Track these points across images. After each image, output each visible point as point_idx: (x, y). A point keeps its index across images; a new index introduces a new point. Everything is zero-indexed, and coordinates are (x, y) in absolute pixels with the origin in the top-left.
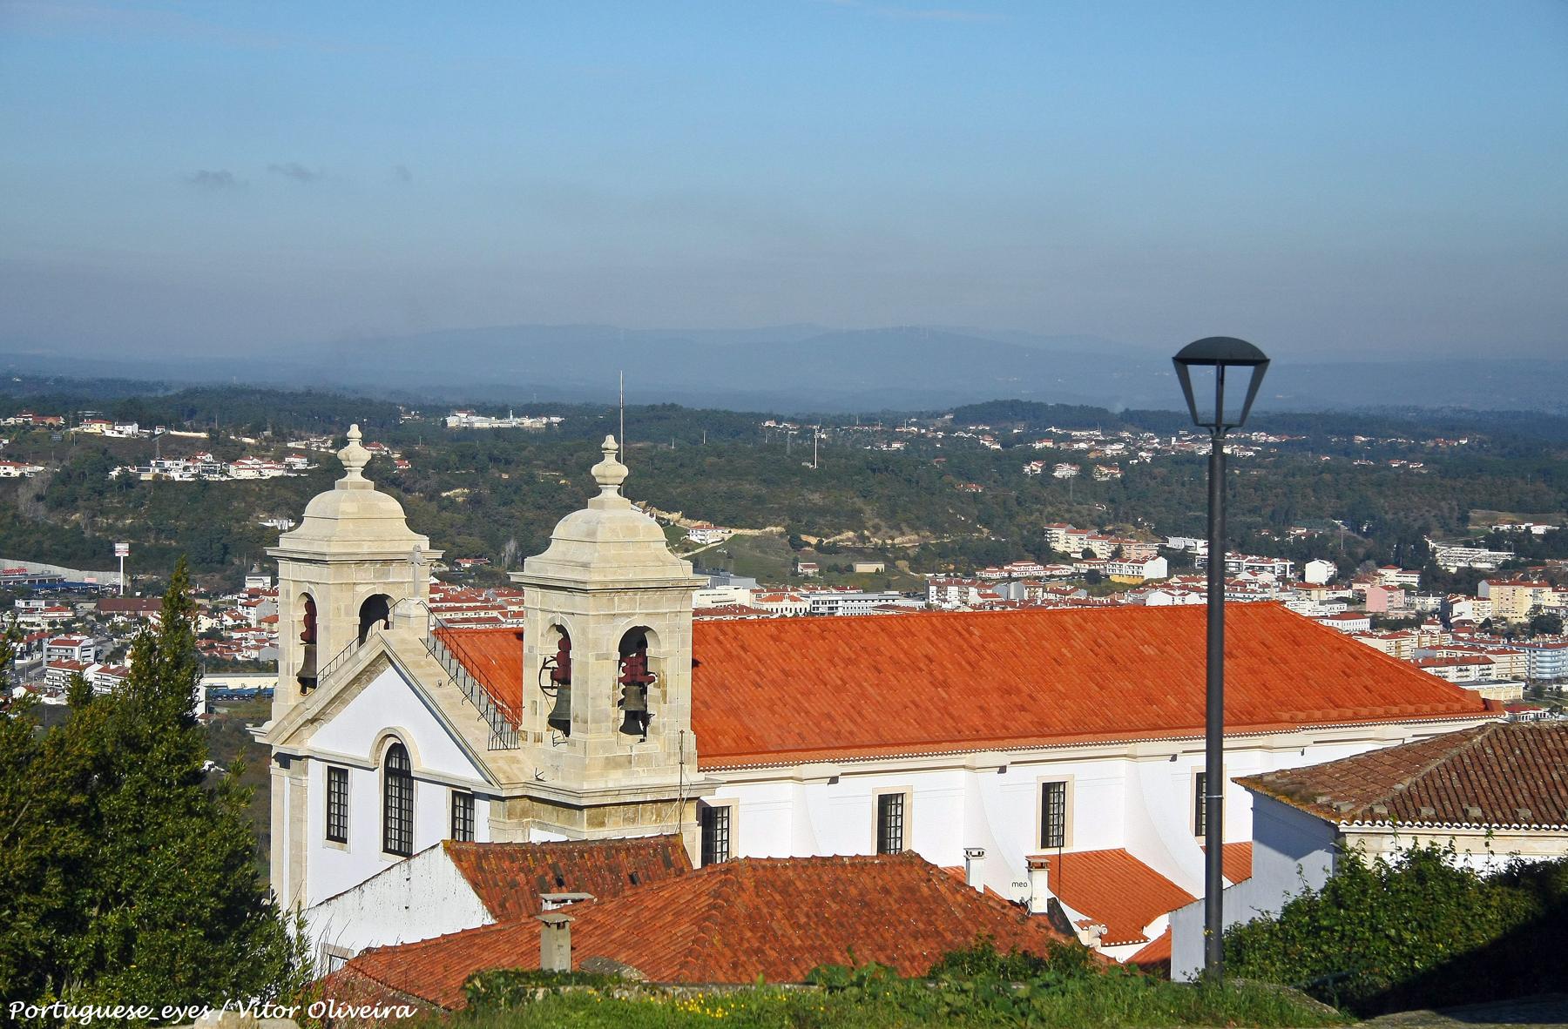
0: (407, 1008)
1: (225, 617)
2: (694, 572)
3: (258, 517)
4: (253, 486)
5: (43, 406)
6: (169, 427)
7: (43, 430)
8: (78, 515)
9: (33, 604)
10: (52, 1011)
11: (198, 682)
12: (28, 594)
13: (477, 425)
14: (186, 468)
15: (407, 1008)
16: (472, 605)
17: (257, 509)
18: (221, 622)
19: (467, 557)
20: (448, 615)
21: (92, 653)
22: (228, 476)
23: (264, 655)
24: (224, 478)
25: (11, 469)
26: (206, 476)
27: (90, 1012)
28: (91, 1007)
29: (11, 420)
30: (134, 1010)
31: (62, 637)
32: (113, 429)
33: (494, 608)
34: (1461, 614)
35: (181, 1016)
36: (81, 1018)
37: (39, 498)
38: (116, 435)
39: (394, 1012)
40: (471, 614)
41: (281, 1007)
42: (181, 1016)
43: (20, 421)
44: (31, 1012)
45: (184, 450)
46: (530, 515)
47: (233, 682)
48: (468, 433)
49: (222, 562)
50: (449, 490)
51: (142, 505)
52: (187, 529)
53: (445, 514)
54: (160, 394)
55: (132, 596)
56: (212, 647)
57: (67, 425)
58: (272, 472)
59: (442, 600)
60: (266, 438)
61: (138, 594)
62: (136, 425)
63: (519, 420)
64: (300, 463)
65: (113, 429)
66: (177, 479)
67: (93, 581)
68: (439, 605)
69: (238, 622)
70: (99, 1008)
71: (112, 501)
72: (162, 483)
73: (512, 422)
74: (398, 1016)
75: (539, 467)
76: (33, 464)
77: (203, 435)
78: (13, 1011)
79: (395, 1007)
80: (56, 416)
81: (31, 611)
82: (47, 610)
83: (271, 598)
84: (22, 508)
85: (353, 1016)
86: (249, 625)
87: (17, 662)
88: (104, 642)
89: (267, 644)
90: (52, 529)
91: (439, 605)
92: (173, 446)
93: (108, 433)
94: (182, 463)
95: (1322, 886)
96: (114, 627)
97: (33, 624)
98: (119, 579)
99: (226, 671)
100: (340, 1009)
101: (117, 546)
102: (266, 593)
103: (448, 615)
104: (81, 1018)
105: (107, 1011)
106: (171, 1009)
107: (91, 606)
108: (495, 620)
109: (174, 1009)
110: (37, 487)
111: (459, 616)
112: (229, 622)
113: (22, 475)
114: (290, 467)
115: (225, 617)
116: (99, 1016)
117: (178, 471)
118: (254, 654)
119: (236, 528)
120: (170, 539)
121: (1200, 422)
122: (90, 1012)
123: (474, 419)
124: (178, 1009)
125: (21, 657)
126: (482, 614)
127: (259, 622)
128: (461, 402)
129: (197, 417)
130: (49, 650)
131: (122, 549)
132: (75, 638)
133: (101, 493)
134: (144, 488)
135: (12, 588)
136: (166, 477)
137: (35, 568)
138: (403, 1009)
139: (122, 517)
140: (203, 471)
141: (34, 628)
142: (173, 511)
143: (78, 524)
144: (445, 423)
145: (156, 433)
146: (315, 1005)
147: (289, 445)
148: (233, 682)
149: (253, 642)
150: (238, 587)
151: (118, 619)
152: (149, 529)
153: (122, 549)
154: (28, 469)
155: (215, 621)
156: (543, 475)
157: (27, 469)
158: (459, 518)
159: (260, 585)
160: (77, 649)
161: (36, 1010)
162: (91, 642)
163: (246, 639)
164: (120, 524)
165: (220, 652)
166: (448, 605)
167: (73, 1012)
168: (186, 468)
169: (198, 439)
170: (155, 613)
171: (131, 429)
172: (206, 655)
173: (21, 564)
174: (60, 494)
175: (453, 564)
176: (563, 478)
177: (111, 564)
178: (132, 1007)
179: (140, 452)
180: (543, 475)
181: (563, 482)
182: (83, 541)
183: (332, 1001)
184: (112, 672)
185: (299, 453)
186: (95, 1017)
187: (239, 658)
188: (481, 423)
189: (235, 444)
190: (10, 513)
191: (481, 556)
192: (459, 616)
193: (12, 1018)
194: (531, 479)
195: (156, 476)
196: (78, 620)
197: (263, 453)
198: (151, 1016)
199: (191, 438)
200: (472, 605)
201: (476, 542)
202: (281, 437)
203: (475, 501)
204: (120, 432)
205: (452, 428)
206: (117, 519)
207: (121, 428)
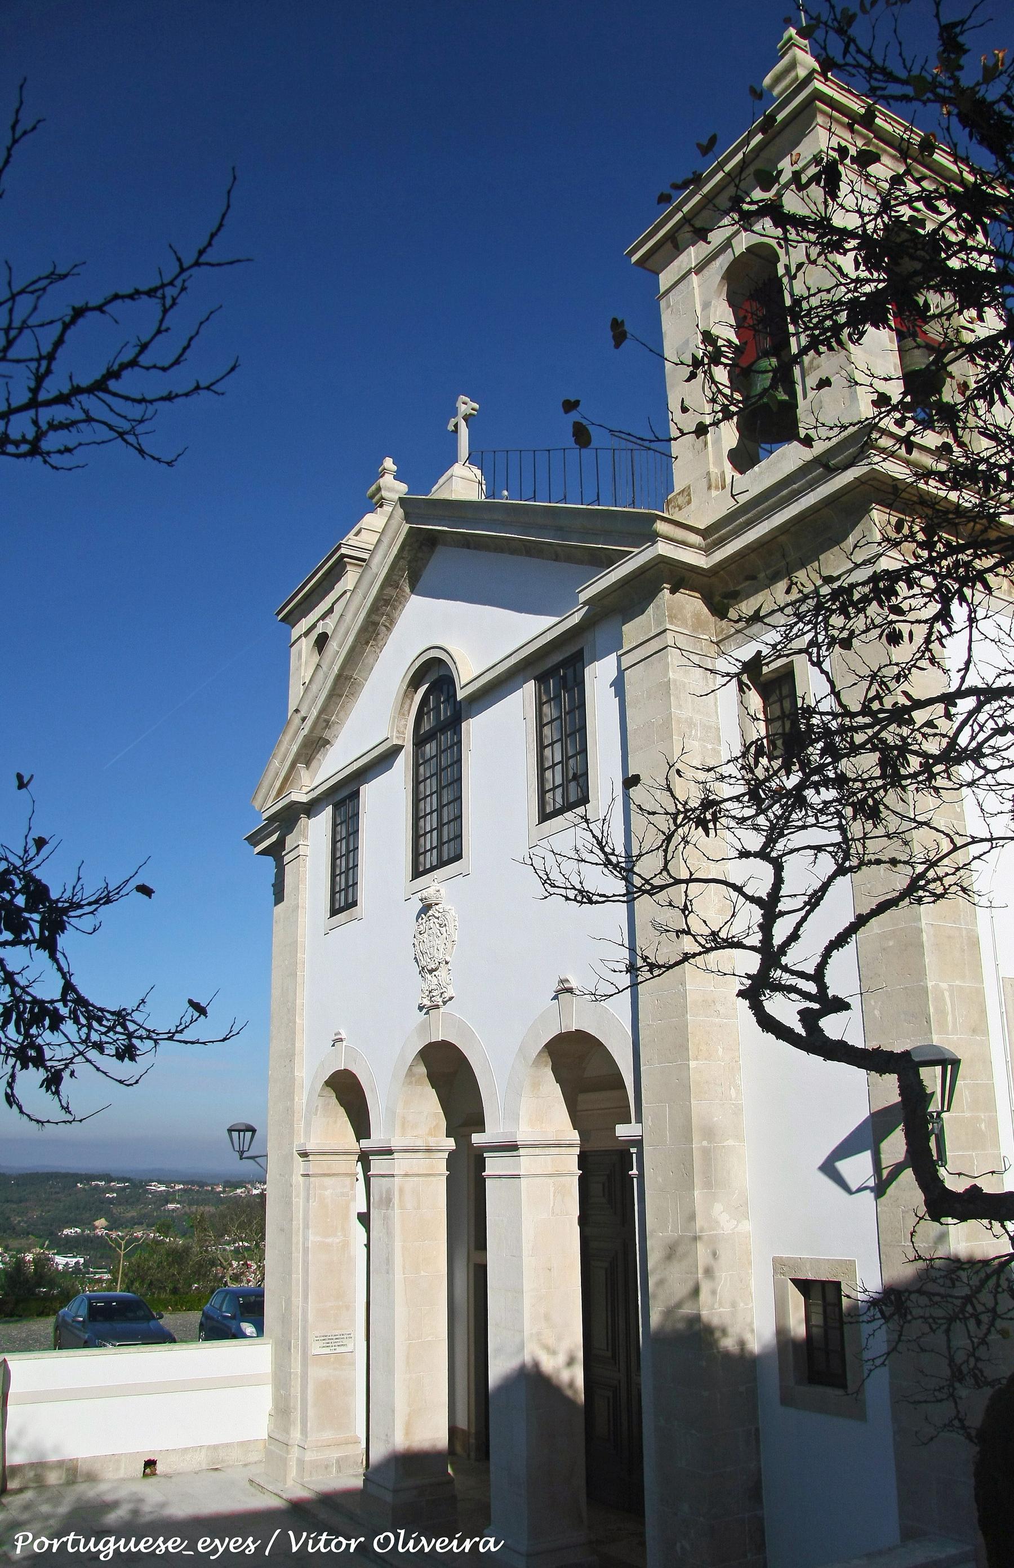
0: (492, 1540)
2: (839, 1283)
10: (66, 1543)
11: (985, 1378)
28: (112, 1539)
30: (164, 1542)
35: (221, 1550)
39: (477, 1544)
44: (339, 1545)
70: (123, 1540)
74: (482, 1550)
78: (20, 1544)
79: (477, 1539)
85: (427, 1550)
95: (39, 997)
104: (100, 1552)
105: (132, 1544)
109: (212, 1542)
116: (122, 1550)
121: (854, 1188)
122: (111, 1544)
124: (217, 1541)
128: (155, 1179)
138: (487, 1543)
146: (382, 1537)
161: (344, 1542)
167: (132, 1544)
178: (161, 1539)
183: (402, 1532)
186: (117, 1551)
198: (184, 1549)
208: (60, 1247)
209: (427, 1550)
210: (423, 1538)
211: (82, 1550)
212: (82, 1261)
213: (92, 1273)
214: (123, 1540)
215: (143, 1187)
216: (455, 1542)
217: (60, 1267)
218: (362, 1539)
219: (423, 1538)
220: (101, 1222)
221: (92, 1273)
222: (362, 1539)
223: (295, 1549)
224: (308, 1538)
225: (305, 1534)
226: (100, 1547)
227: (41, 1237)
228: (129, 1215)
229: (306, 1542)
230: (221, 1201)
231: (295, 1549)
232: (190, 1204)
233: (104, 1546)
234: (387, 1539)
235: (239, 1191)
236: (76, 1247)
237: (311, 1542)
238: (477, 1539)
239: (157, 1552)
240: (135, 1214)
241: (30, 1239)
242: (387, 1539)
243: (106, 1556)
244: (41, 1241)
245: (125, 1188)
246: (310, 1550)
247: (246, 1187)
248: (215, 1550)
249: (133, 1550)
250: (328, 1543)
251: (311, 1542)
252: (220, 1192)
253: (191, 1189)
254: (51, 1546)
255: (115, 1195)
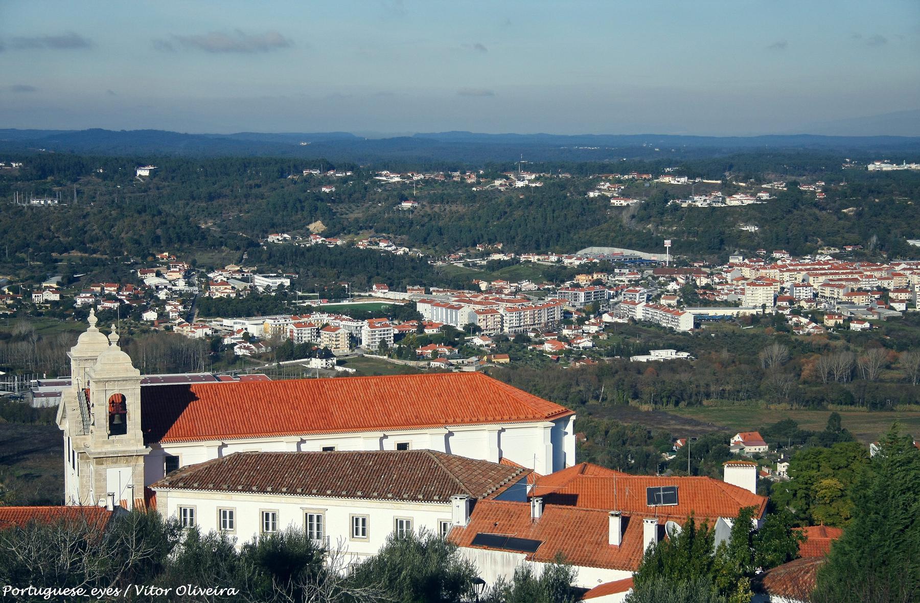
0: (234, 589)
1: (715, 278)
3: (739, 225)
4: (738, 209)
5: (642, 170)
6: (703, 178)
7: (641, 181)
8: (650, 225)
9: (623, 271)
10: (28, 591)
12: (621, 265)
13: (884, 169)
14: (705, 200)
15: (234, 589)
16: (845, 271)
17: (739, 221)
18: (713, 280)
19: (850, 245)
20: (831, 277)
21: (645, 296)
22: (725, 204)
23: (731, 298)
24: (724, 205)
25: (622, 202)
26: (714, 205)
27: (49, 591)
28: (50, 589)
29: (626, 177)
31: (631, 288)
32: (675, 180)
33: (856, 273)
34: (255, 538)
35: (102, 594)
36: (44, 595)
37: (633, 217)
38: (676, 183)
39: (226, 591)
40: (844, 277)
41: (160, 589)
42: (102, 594)
43: (631, 177)
44: (159, 592)
45: (705, 190)
46: (889, 221)
47: (712, 312)
48: (880, 173)
49: (720, 249)
50: (846, 209)
51: (681, 220)
52: (703, 232)
53: (841, 222)
54: (717, 156)
55: (672, 267)
56: (705, 293)
57: (652, 179)
58: (748, 201)
59: (829, 269)
60: (751, 183)
61: (675, 266)
62: (686, 178)
63: (908, 165)
64: (765, 196)
65: (675, 180)
66: (700, 206)
67: (655, 258)
68: (827, 271)
69: (721, 280)
70: (55, 589)
71: (668, 218)
72: (691, 208)
73: (905, 166)
74: (228, 594)
75: (896, 195)
76: (633, 199)
77: (719, 182)
78: (5, 591)
79: (226, 589)
80: (647, 173)
81: (621, 274)
82: (629, 274)
83: (739, 268)
84: (625, 221)
86: (727, 282)
87: (611, 300)
88: (654, 290)
89: (733, 292)
90: (638, 232)
91: (827, 271)
92: (703, 188)
93: (672, 182)
94: (704, 198)
96: (659, 283)
97: (621, 281)
98: (667, 257)
99: (710, 306)
100: (195, 590)
101: (665, 241)
102: (737, 265)
103: (831, 277)
104: (44, 595)
105: (59, 591)
106: (96, 590)
107: (651, 272)
108: (856, 280)
110: (631, 211)
111: (837, 277)
112: (717, 280)
113: (628, 205)
114: (759, 199)
115: (715, 278)
116: (55, 594)
117: (700, 202)
118: (725, 297)
119: (727, 231)
120: (694, 237)
122: (49, 591)
123: (883, 165)
124: (101, 590)
125: (613, 298)
126: (850, 276)
127: (732, 281)
129: (733, 169)
130: (624, 294)
131: (668, 243)
132: (638, 289)
133: (662, 214)
134: (683, 211)
135: (615, 262)
136: (695, 205)
137: (628, 252)
138: (231, 591)
139: (671, 226)
140: (713, 202)
141: (622, 283)
142: (696, 222)
143: (650, 230)
144: (867, 168)
145: (696, 181)
146: (180, 588)
147: (763, 186)
148: (712, 312)
149: (726, 291)
150: (725, 261)
151: (661, 279)
152: (684, 232)
153: (668, 243)
154: (631, 202)
155: (709, 280)
156: (898, 199)
157: (630, 202)
158: (848, 224)
159: (737, 261)
160: (638, 295)
162: (645, 290)
163: (723, 289)
164: (670, 230)
165: (709, 297)
166: (832, 271)
167: (40, 591)
168: (705, 200)
169: (717, 184)
170: (681, 276)
171: (683, 180)
172: (701, 297)
173: (622, 250)
174: (645, 213)
175: (842, 248)
176: (910, 200)
177: (663, 250)
179: (685, 192)
180: (898, 199)
181: (910, 203)
182: (651, 238)
183: (190, 586)
184: (650, 307)
185: (766, 190)
187: (718, 299)
188: (887, 167)
189: (735, 186)
190: (619, 224)
191: (858, 244)
192: (837, 277)
193: (5, 595)
194: (893, 202)
195: (690, 205)
196: (643, 279)
197: (748, 191)
198: (84, 594)
199: (714, 183)
200: (845, 271)
201: (854, 236)
202: (760, 181)
203: (859, 215)
204: (678, 182)
205: (871, 171)
206: (668, 227)
207: (679, 179)
208: (262, 262)
209: (202, 594)
210: (200, 589)
211: (35, 594)
212: (287, 282)
213: (301, 298)
214: (55, 589)
215: (369, 177)
216: (216, 591)
217: (261, 289)
218: (171, 589)
219: (200, 589)
220: (317, 226)
221: (301, 298)
222: (171, 589)
223: (138, 594)
224: (145, 588)
225: (143, 587)
226: (44, 593)
227: (238, 248)
228: (352, 216)
229: (144, 590)
230: (473, 197)
231: (138, 594)
232: (432, 202)
233: (46, 592)
234: (183, 589)
235: (497, 183)
236: (282, 263)
237: (146, 590)
238: (226, 589)
239: (115, 595)
240: (360, 215)
241: (223, 251)
242: (183, 589)
243: (47, 597)
244: (238, 254)
245: (345, 180)
246: (145, 594)
247: (508, 178)
248: (100, 594)
249: (60, 594)
250: (154, 591)
251: (146, 590)
252: (472, 185)
253: (434, 180)
254: (164, 592)
255: (334, 189)
